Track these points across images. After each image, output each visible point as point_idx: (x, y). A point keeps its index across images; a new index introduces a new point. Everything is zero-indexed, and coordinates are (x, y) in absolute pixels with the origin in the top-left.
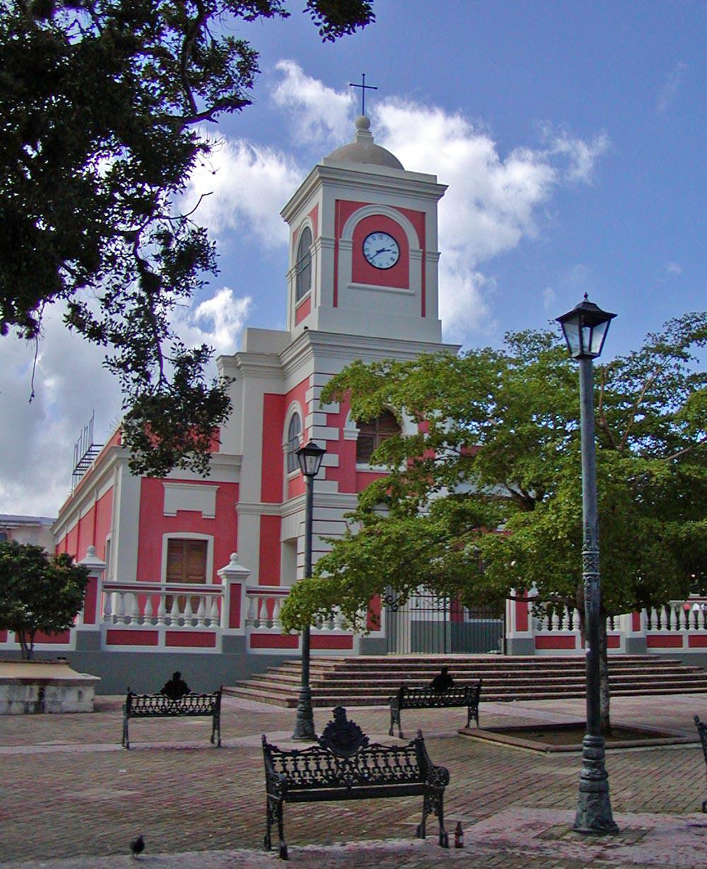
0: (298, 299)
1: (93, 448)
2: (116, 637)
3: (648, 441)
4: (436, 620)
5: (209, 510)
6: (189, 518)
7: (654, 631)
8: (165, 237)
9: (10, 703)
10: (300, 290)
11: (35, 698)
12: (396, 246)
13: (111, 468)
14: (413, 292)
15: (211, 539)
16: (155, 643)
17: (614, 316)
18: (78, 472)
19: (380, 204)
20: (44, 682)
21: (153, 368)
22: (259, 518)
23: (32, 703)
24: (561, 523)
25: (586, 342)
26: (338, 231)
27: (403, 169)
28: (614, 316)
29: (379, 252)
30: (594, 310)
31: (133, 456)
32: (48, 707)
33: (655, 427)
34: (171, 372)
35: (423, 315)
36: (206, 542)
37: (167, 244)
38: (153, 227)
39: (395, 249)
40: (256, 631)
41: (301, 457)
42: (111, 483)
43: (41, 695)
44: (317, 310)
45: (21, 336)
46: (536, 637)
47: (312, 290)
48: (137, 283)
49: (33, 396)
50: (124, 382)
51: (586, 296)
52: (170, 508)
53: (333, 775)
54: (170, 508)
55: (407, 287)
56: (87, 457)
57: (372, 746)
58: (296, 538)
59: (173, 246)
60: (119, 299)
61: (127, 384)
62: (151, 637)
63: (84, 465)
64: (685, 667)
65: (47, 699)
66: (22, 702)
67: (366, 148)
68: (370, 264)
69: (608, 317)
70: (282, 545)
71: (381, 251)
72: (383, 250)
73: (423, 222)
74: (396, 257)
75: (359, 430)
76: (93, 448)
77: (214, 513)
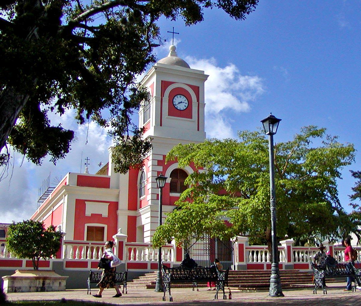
0: (144, 123)
1: (50, 189)
2: (70, 264)
3: (293, 174)
4: (205, 259)
5: (105, 214)
6: (96, 217)
7: (297, 262)
8: (134, 90)
9: (30, 287)
10: (145, 120)
11: (41, 285)
12: (187, 100)
13: (62, 195)
14: (194, 120)
15: (106, 226)
16: (87, 267)
17: (281, 120)
18: (41, 201)
19: (180, 83)
20: (45, 279)
21: (125, 135)
22: (127, 217)
23: (39, 287)
24: (260, 203)
25: (271, 130)
26: (162, 94)
27: (190, 68)
28: (281, 120)
29: (179, 103)
30: (274, 118)
31: (115, 166)
32: (46, 288)
33: (295, 168)
34: (132, 136)
35: (198, 130)
36: (103, 228)
37: (135, 92)
38: (130, 86)
39: (187, 102)
40: (129, 262)
41: (158, 181)
42: (62, 201)
43: (44, 284)
44: (153, 127)
45: (78, 123)
46: (247, 264)
47: (151, 119)
48: (122, 105)
49: (87, 142)
50: (114, 139)
51: (271, 113)
52: (88, 213)
53: (186, 276)
54: (88, 213)
55: (191, 118)
56: (46, 193)
57: (199, 267)
58: (144, 225)
59: (137, 92)
60: (116, 110)
61: (115, 140)
62: (85, 264)
63: (44, 197)
64: (310, 274)
65: (46, 285)
66: (36, 287)
67: (174, 59)
68: (176, 108)
69: (278, 121)
70: (137, 229)
71: (181, 103)
72: (182, 102)
73: (198, 90)
74: (187, 105)
75: (171, 178)
76: (50, 189)
77: (107, 215)
